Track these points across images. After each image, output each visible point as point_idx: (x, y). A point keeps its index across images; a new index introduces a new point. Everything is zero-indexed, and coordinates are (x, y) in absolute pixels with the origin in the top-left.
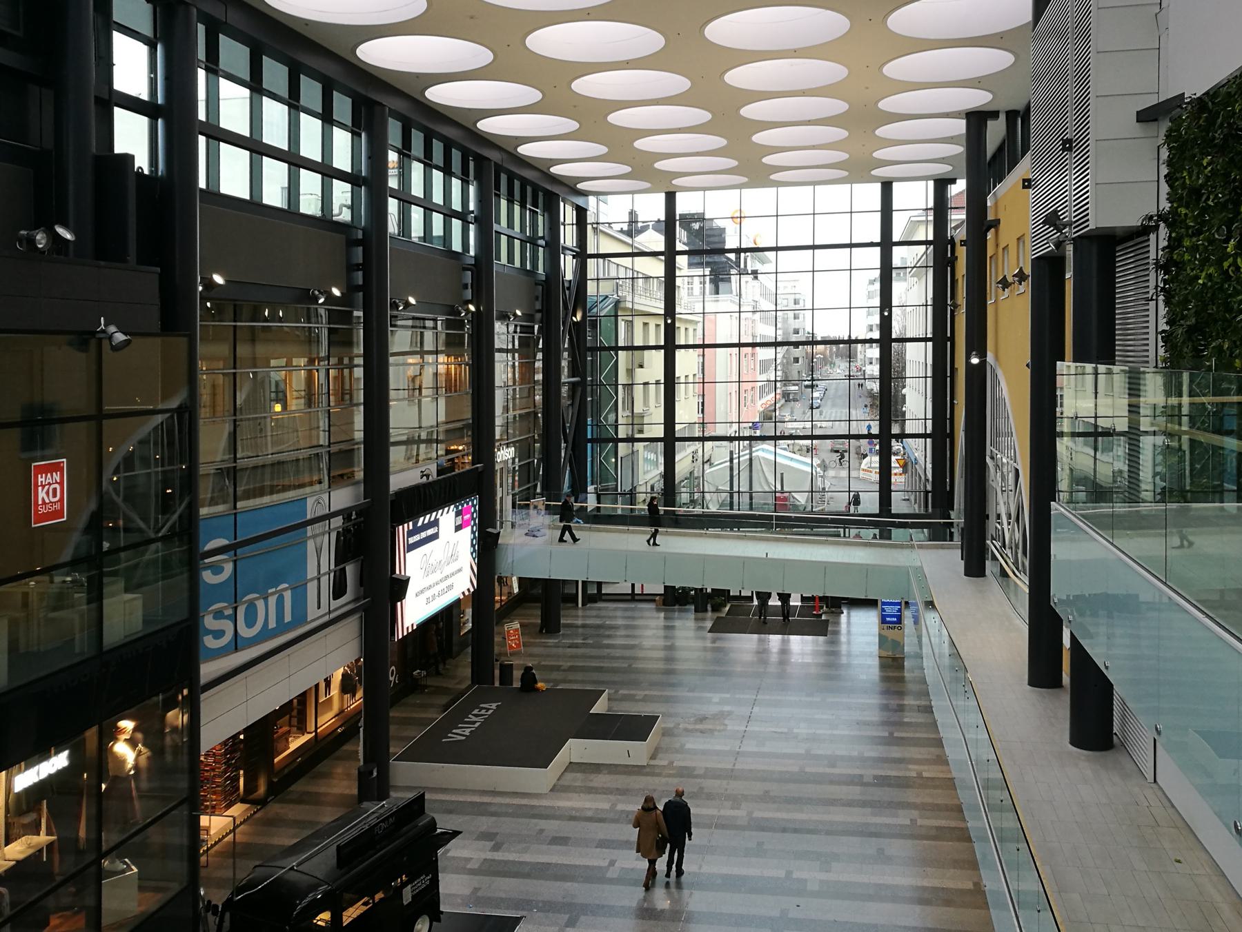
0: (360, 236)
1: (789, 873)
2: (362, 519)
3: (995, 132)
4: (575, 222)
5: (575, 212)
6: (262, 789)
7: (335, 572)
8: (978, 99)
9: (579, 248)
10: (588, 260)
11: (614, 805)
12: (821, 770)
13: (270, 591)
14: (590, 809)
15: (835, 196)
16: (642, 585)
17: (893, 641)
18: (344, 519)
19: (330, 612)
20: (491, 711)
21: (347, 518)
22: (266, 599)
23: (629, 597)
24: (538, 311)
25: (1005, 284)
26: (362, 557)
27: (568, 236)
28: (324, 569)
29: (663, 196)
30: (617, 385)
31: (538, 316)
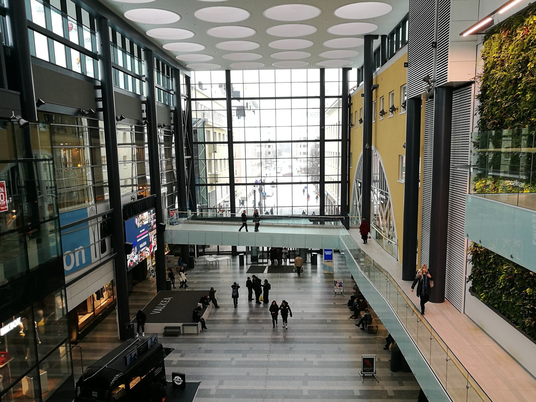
0: (100, 85)
1: (305, 359)
2: (110, 218)
3: (376, 43)
4: (185, 83)
5: (184, 79)
6: (74, 337)
7: (101, 241)
8: (370, 29)
9: (188, 96)
10: (192, 101)
11: (228, 336)
12: (310, 318)
13: (76, 250)
14: (219, 338)
15: (299, 74)
16: (218, 246)
17: (329, 267)
18: (102, 217)
19: (100, 259)
20: (168, 301)
21: (104, 217)
22: (74, 253)
23: (217, 253)
24: (172, 124)
25: (383, 113)
26: (111, 235)
27: (183, 90)
28: (97, 240)
29: (224, 72)
30: (206, 160)
31: (172, 127)
